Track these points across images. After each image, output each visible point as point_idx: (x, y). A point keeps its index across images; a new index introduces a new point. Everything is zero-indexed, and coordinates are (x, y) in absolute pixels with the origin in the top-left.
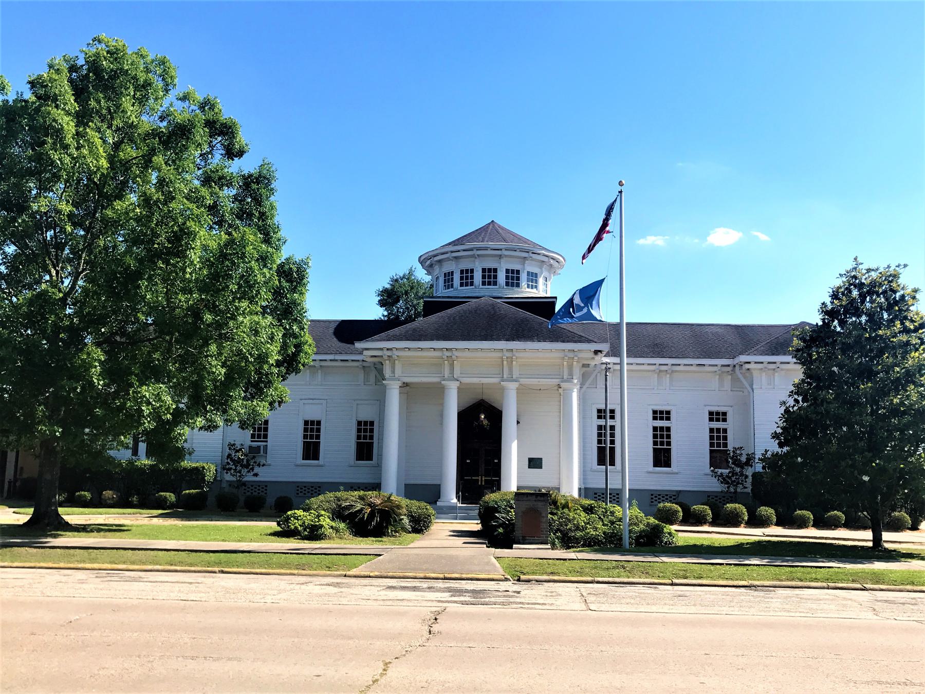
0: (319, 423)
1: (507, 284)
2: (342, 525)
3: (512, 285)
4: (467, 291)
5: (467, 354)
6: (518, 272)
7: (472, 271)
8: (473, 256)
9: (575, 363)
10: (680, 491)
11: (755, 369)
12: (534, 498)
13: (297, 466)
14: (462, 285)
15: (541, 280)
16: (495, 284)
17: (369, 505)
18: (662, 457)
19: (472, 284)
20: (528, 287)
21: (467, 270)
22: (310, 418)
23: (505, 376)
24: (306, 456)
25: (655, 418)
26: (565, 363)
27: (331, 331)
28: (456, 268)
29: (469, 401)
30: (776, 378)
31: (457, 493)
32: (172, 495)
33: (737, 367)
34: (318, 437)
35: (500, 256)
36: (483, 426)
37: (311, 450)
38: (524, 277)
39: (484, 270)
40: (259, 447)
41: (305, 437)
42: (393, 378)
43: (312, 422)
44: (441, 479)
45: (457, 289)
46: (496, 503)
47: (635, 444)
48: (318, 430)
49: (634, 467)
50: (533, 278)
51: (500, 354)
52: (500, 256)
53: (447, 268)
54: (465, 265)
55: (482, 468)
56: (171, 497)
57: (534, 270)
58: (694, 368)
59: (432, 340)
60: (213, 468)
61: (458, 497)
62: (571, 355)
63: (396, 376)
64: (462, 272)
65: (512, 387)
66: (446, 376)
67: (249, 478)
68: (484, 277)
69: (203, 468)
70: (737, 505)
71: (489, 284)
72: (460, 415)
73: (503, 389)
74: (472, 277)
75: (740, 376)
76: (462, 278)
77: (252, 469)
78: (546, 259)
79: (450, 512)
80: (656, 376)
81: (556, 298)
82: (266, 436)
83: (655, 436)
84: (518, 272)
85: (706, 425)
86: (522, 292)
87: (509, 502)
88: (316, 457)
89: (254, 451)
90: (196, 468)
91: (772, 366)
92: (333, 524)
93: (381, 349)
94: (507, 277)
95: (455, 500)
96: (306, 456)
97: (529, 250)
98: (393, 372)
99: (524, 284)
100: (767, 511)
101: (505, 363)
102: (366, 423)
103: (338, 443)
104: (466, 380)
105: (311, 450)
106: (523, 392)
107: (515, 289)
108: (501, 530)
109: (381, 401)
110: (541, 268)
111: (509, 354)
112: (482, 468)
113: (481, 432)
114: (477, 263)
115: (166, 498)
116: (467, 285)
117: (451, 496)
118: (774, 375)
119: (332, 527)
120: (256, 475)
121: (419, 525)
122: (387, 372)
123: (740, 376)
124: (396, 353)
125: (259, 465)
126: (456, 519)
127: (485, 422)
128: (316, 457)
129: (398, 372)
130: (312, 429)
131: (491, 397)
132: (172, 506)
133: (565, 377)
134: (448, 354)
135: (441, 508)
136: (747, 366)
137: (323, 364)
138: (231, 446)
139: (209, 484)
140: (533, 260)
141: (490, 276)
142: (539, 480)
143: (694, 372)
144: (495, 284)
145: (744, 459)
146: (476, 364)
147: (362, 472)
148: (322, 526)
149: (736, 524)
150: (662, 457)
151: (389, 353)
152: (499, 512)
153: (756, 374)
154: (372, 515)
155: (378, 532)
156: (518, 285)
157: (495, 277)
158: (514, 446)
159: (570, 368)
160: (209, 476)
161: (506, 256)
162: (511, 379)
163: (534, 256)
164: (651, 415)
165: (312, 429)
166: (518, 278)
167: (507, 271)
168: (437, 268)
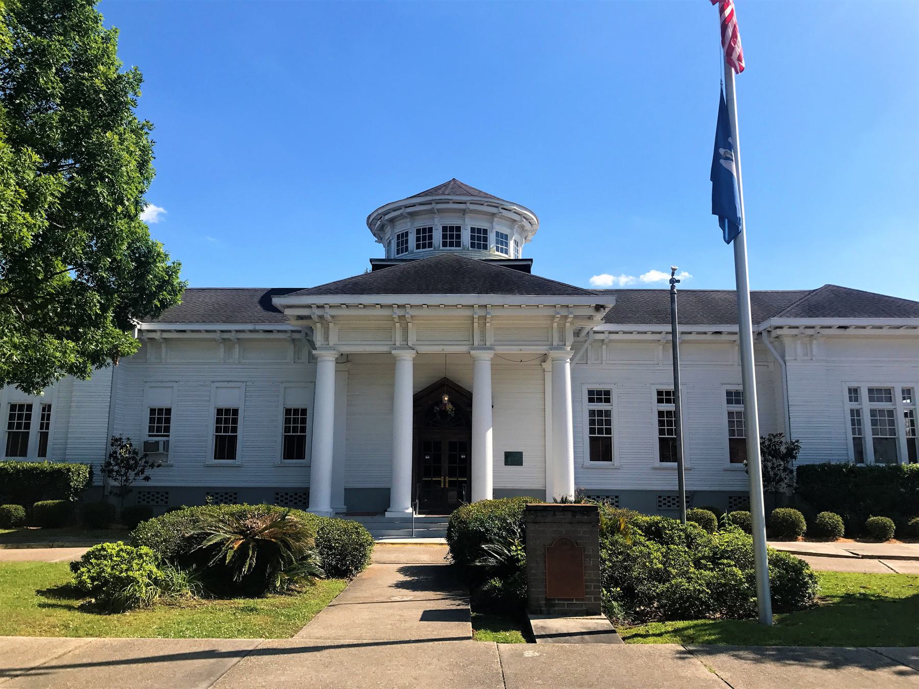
0: (236, 412)
1: (473, 245)
2: (179, 577)
3: (479, 247)
4: (424, 254)
5: (425, 312)
6: (485, 231)
7: (431, 230)
8: (431, 212)
9: (568, 324)
10: (695, 492)
11: (786, 336)
12: (569, 515)
13: (208, 466)
14: (418, 247)
15: (512, 244)
16: (458, 244)
17: (241, 533)
18: (669, 449)
19: (430, 245)
20: (497, 250)
21: (424, 230)
22: (224, 405)
23: (476, 343)
24: (219, 455)
25: (660, 401)
26: (555, 325)
27: (256, 299)
28: (410, 227)
29: (427, 380)
30: (814, 347)
31: (413, 500)
32: (20, 507)
33: (765, 334)
34: (234, 430)
35: (464, 212)
36: (445, 412)
37: (226, 446)
38: (492, 238)
39: (445, 229)
40: (157, 443)
41: (218, 429)
42: (327, 347)
43: (227, 411)
44: (750, 486)
45: (412, 252)
46: (482, 523)
47: (635, 432)
48: (235, 421)
49: (635, 462)
50: (503, 240)
51: (468, 312)
52: (464, 212)
53: (400, 228)
54: (421, 223)
55: (445, 465)
56: (18, 510)
57: (505, 230)
58: (709, 337)
59: (378, 293)
60: (85, 470)
61: (414, 505)
62: (564, 312)
63: (331, 343)
64: (418, 231)
65: (485, 359)
66: (398, 344)
67: (140, 483)
68: (444, 237)
69: (69, 470)
70: (792, 511)
71: (451, 245)
72: (419, 399)
73: (474, 360)
74: (431, 237)
75: (769, 345)
76: (418, 239)
77: (142, 471)
78: (517, 217)
79: (404, 526)
80: (661, 347)
81: (531, 260)
82: (167, 429)
83: (661, 423)
84: (485, 231)
85: (725, 408)
86: (490, 255)
87: (505, 520)
88: (232, 456)
89: (150, 447)
90: (59, 470)
91: (810, 332)
92: (159, 574)
93: (309, 307)
94: (472, 238)
95: (410, 510)
96: (219, 455)
97: (495, 206)
98: (327, 338)
99: (492, 245)
100: (830, 517)
101: (476, 325)
102: (296, 411)
103: (260, 436)
104: (424, 349)
105: (226, 446)
106: (497, 369)
107: (484, 251)
108: (496, 583)
109: (311, 382)
110: (512, 228)
111: (482, 312)
112: (445, 465)
113: (445, 420)
114: (436, 220)
115: (9, 511)
116: (424, 247)
117: (404, 504)
118: (811, 344)
119: (156, 582)
120: (147, 479)
121: (344, 563)
122: (318, 339)
123: (769, 345)
124: (330, 312)
125: (152, 466)
126: (411, 536)
127: (449, 407)
128: (232, 456)
129: (333, 339)
130: (227, 418)
131: (459, 376)
132: (19, 523)
133: (555, 343)
134: (400, 312)
135: (392, 520)
136: (779, 332)
137: (241, 336)
138: (116, 441)
139: (77, 492)
140: (503, 217)
141: (452, 235)
142: (517, 478)
143: (710, 342)
144: (458, 244)
145: (783, 449)
146: (435, 327)
147: (286, 476)
148: (130, 580)
149: (792, 537)
150: (669, 449)
151: (319, 312)
152: (491, 541)
153: (787, 342)
154: (242, 554)
155: (256, 586)
156: (485, 247)
157: (459, 236)
158: (489, 434)
159: (562, 330)
160: (77, 482)
161: (472, 211)
162: (484, 347)
163: (505, 213)
164: (655, 397)
165: (227, 418)
166: (485, 239)
167: (473, 230)
168: (388, 229)
